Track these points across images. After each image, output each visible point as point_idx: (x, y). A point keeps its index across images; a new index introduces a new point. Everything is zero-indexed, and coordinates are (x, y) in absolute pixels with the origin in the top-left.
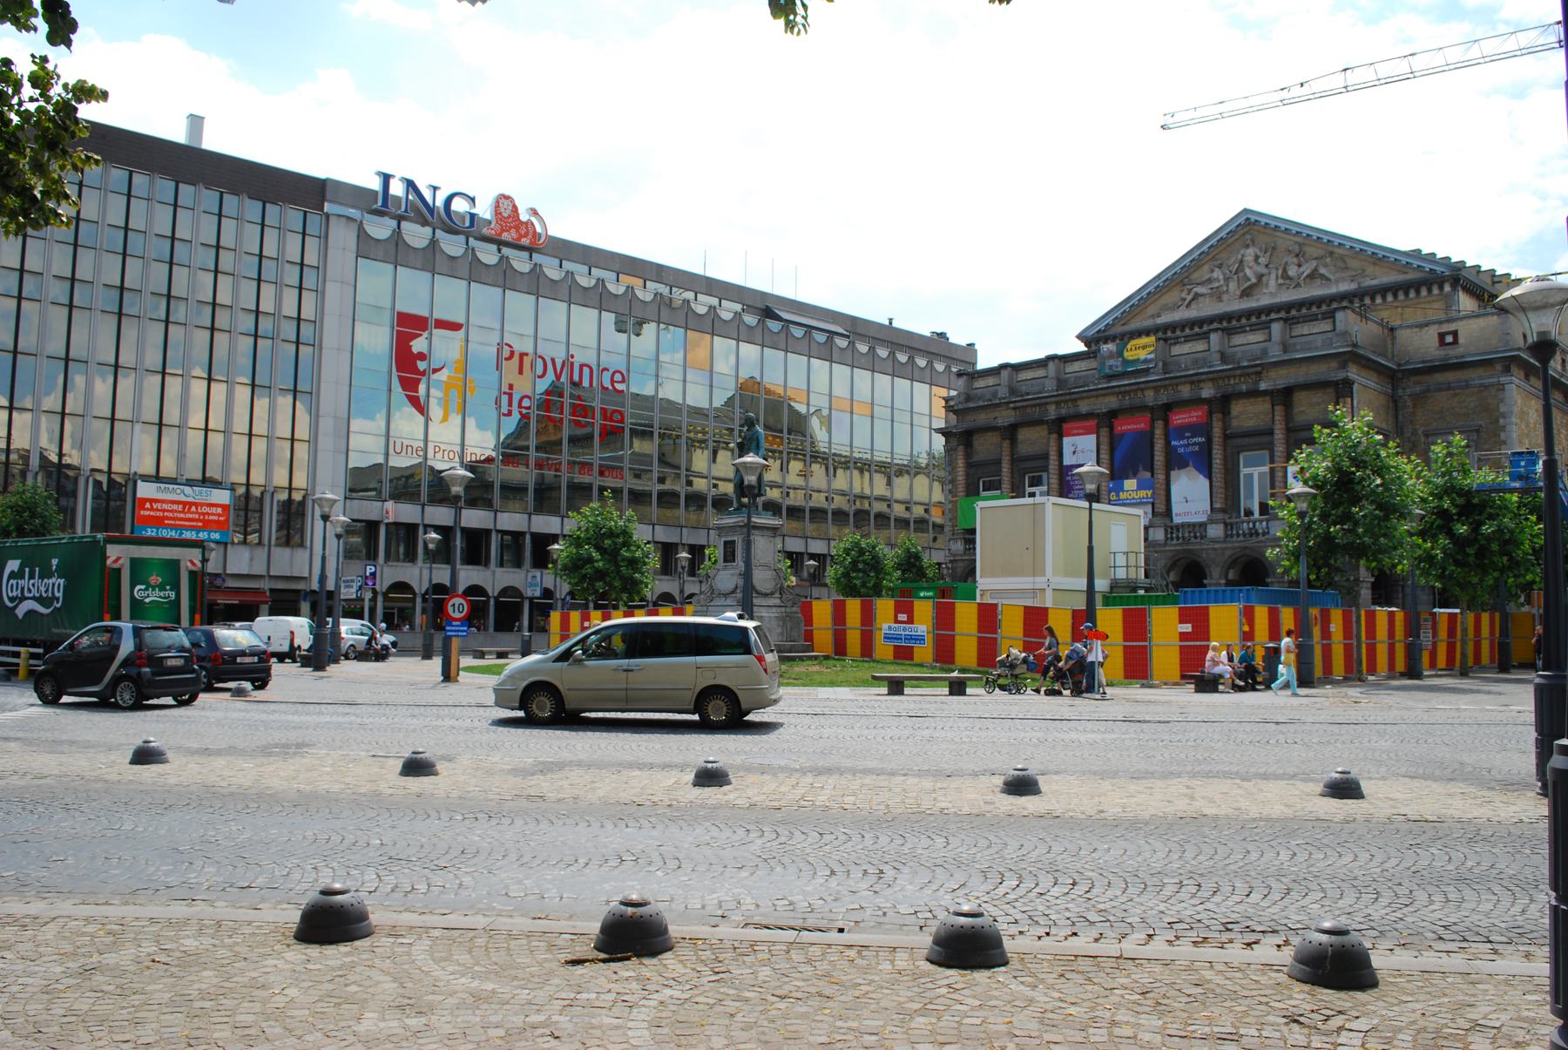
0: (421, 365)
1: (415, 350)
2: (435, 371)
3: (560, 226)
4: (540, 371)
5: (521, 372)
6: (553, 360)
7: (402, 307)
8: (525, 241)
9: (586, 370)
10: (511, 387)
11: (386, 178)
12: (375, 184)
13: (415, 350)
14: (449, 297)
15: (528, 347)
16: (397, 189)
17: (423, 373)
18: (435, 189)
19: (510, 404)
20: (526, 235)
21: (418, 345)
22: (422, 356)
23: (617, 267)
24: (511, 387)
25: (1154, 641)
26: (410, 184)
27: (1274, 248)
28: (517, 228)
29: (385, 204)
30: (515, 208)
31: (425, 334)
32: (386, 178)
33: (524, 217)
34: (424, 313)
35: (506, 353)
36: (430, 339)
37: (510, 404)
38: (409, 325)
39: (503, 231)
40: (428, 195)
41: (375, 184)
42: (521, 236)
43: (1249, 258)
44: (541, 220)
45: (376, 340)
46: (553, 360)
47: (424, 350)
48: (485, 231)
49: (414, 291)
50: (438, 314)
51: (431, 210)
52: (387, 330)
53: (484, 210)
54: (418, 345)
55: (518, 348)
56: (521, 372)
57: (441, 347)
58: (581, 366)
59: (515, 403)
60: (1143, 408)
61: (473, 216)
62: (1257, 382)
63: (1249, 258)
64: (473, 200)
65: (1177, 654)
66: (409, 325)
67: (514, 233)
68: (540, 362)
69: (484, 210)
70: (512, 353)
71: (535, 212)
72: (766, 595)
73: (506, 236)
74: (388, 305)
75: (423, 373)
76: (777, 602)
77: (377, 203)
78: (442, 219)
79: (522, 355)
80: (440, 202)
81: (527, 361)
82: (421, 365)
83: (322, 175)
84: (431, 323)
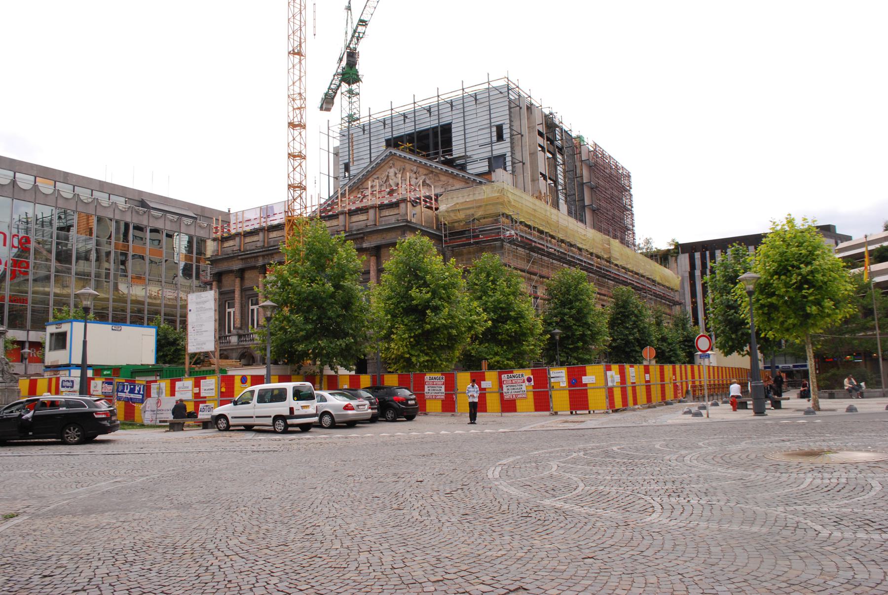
23: (35, 173)
60: (232, 271)
62: (361, 244)
63: (392, 174)
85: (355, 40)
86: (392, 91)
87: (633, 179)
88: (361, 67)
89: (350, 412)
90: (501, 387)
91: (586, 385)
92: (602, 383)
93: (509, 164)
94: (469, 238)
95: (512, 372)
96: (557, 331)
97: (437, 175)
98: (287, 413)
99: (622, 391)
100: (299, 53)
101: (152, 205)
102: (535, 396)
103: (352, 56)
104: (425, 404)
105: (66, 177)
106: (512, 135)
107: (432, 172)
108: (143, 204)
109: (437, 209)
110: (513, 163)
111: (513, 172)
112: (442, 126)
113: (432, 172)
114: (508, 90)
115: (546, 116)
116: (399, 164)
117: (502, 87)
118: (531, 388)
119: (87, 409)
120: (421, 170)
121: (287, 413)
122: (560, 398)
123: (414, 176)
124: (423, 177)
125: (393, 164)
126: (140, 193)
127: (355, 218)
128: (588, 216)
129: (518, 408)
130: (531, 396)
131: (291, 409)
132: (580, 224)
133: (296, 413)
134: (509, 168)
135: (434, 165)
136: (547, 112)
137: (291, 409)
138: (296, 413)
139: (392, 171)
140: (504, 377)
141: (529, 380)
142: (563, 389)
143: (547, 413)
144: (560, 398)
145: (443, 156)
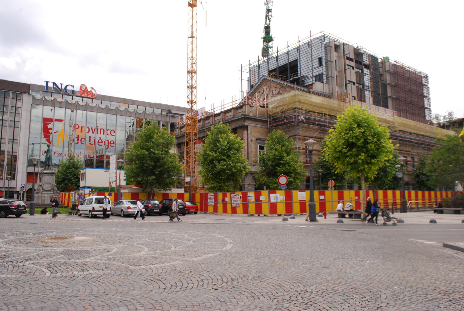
0: (50, 131)
1: (49, 127)
2: (55, 133)
3: (101, 92)
4: (87, 131)
5: (81, 131)
6: (92, 128)
7: (45, 116)
8: (90, 96)
9: (102, 131)
10: (78, 136)
11: (47, 83)
12: (44, 84)
13: (49, 127)
14: (60, 113)
15: (84, 125)
16: (50, 85)
17: (51, 133)
18: (62, 84)
19: (78, 140)
20: (90, 94)
21: (49, 126)
22: (51, 129)
23: (119, 101)
24: (78, 136)
25: (294, 201)
26: (54, 84)
27: (270, 86)
28: (87, 93)
29: (47, 89)
30: (86, 88)
31: (52, 123)
32: (47, 83)
33: (89, 90)
34: (52, 118)
35: (77, 126)
36: (53, 124)
37: (78, 140)
38: (47, 121)
39: (82, 94)
40: (60, 86)
41: (44, 84)
42: (88, 95)
43: (265, 89)
44: (95, 90)
45: (38, 126)
46: (92, 128)
47: (52, 127)
48: (77, 95)
49: (47, 112)
50: (56, 118)
51: (60, 90)
52: (41, 123)
53: (77, 89)
54: (49, 126)
55: (80, 126)
56: (81, 131)
57: (56, 126)
58: (101, 129)
59: (80, 140)
61: (73, 91)
63: (265, 89)
64: (73, 86)
65: (299, 205)
66: (47, 121)
67: (86, 94)
68: (87, 129)
69: (77, 89)
70: (79, 127)
71: (93, 88)
72: (47, 191)
73: (83, 95)
74: (41, 116)
75: (51, 133)
76: (52, 193)
77: (46, 89)
78: (63, 91)
79: (82, 127)
80: (63, 87)
81: (83, 129)
82: (50, 131)
83: (29, 83)
84: (54, 120)
85: (268, 21)
86: (281, 45)
87: (430, 78)
88: (272, 34)
89: (129, 210)
90: (231, 201)
91: (261, 201)
92: (267, 200)
93: (325, 78)
94: (279, 122)
95: (234, 193)
96: (320, 170)
97: (285, 88)
98: (92, 209)
99: (223, 205)
100: (192, 37)
101: (173, 112)
102: (320, 204)
103: (267, 29)
104: (208, 208)
105: (133, 102)
106: (326, 63)
107: (283, 87)
108: (169, 112)
109: (267, 107)
110: (327, 78)
111: (327, 82)
112: (290, 63)
113: (283, 87)
114: (324, 37)
115: (354, 49)
116: (268, 84)
117: (321, 37)
118: (241, 202)
119: (8, 205)
120: (278, 86)
121: (92, 209)
122: (252, 208)
123: (275, 89)
124: (278, 90)
125: (266, 84)
126: (168, 106)
127: (227, 115)
128: (390, 103)
129: (237, 211)
130: (241, 206)
131: (93, 208)
132: (382, 109)
133: (95, 209)
134: (325, 81)
135: (286, 84)
136: (355, 47)
137: (93, 208)
138: (95, 209)
139: (265, 88)
140: (232, 195)
141: (241, 197)
142: (252, 203)
143: (246, 215)
144: (252, 208)
145: (293, 78)
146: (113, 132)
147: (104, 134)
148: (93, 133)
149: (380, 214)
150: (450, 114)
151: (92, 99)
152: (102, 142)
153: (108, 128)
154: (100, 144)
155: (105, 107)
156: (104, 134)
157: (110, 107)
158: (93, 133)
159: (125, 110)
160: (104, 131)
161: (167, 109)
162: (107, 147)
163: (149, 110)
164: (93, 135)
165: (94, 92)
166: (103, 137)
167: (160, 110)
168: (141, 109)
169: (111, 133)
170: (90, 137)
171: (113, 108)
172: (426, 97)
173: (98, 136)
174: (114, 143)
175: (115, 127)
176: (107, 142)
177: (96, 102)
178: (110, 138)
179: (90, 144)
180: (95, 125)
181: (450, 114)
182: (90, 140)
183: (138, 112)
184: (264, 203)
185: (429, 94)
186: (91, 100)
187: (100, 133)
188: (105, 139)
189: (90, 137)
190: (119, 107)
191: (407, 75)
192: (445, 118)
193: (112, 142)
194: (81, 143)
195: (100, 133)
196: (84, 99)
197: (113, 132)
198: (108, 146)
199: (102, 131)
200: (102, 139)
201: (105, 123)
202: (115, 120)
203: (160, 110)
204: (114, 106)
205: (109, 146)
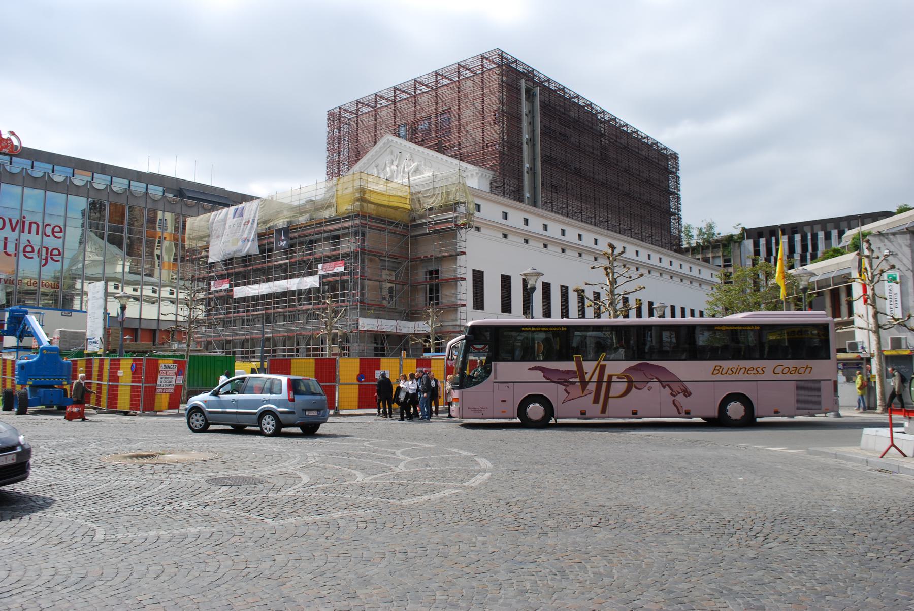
3: (29, 142)
6: (10, 220)
19: (47, 254)
20: (6, 147)
46: (10, 220)
58: (31, 223)
71: (12, 133)
105: (104, 169)
146: (57, 229)
147: (37, 234)
148: (13, 230)
149: (780, 233)
150: (710, 227)
151: (11, 156)
152: (33, 251)
153: (46, 222)
154: (28, 254)
155: (41, 175)
156: (37, 234)
157: (30, 172)
158: (13, 230)
159: (44, 176)
160: (41, 229)
161: (175, 187)
162: (43, 262)
163: (119, 185)
164: (12, 236)
165: (15, 142)
166: (35, 240)
167: (161, 189)
168: (101, 181)
169: (53, 232)
170: (6, 239)
171: (37, 174)
172: (674, 214)
173: (25, 237)
174: (59, 254)
175: (63, 219)
176: (44, 250)
177: (19, 165)
178: (51, 242)
179: (6, 253)
180: (19, 212)
181: (710, 227)
182: (5, 244)
183: (96, 186)
184: (353, 384)
185: (679, 209)
186: (8, 158)
187: (30, 232)
188: (39, 243)
189: (6, 239)
190: (50, 172)
191: (644, 153)
192: (701, 232)
193: (55, 252)
194: (25, 255)
195: (30, 232)
196: (14, 159)
197: (57, 229)
198: (46, 259)
199: (34, 226)
200: (32, 243)
201: (19, 208)
202: (64, 203)
203: (161, 189)
204: (40, 170)
205: (49, 259)
